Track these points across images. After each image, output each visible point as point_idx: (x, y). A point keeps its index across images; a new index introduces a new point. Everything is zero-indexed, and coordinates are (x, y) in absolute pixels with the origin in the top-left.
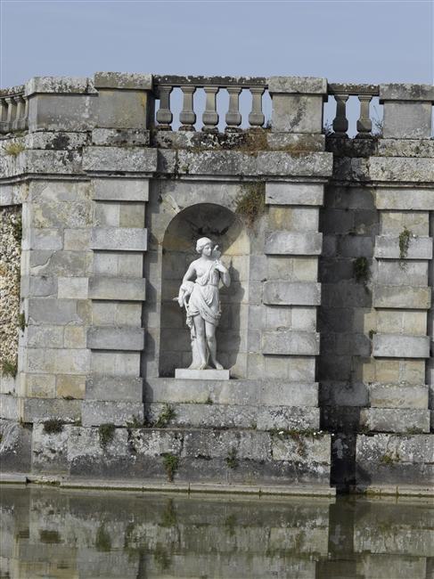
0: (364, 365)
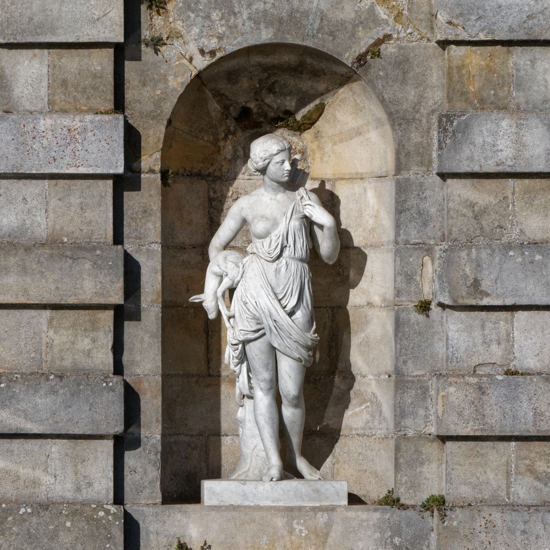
0: (351, 290)
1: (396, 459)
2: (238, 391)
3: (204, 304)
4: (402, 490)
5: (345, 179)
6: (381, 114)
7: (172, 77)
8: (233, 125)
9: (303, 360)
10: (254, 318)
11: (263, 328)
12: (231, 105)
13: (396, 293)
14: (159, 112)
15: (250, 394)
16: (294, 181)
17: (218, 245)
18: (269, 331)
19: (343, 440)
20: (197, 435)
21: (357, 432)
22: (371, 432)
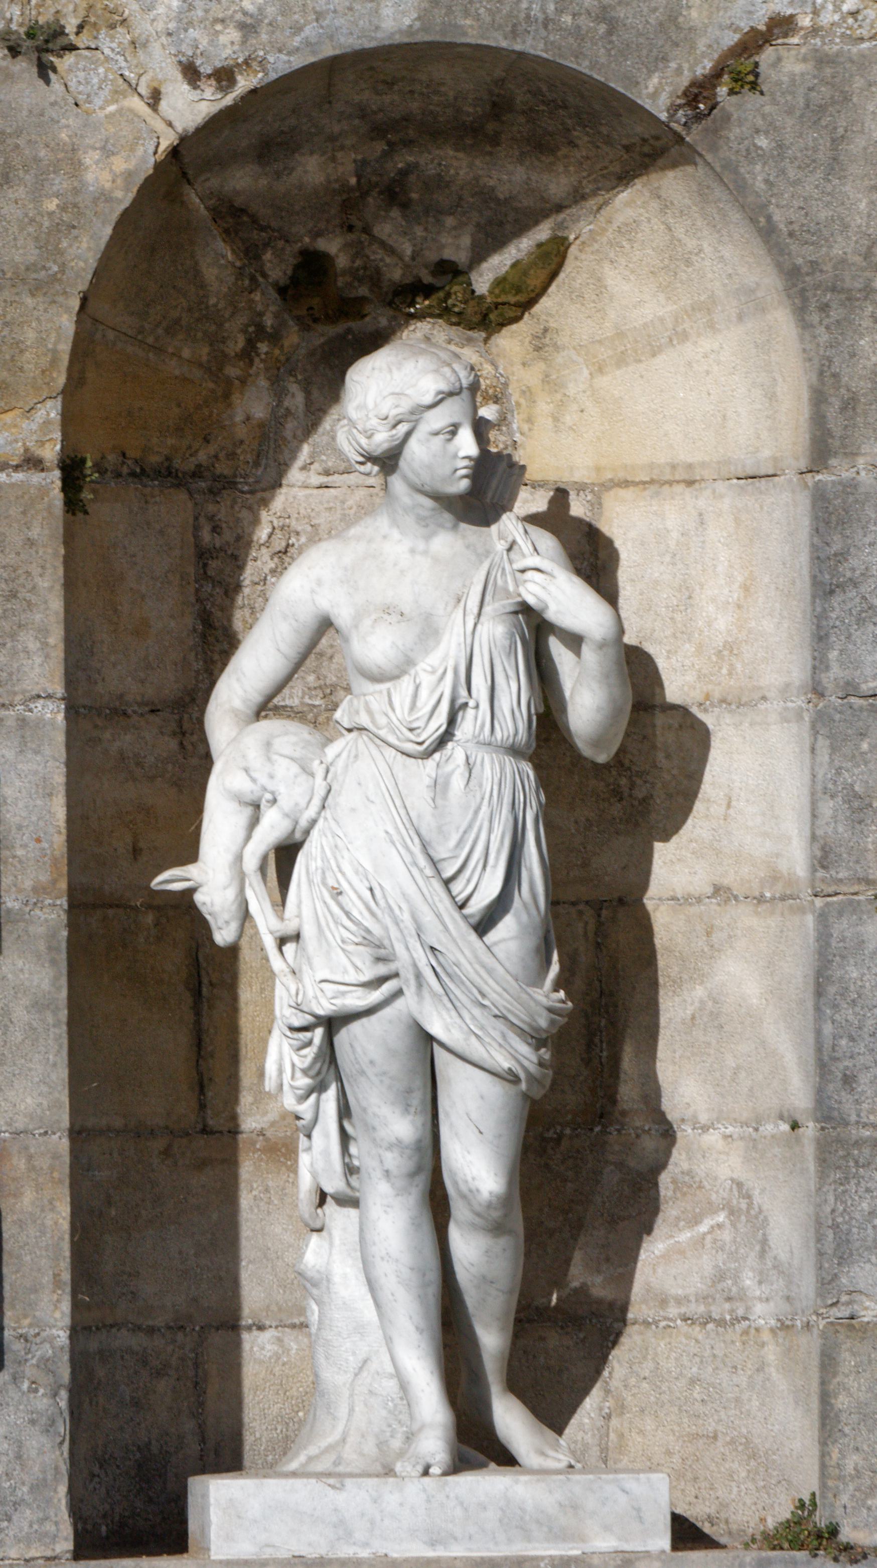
0: (658, 846)
1: (825, 1398)
2: (305, 1181)
3: (199, 898)
4: (845, 1499)
5: (635, 484)
6: (762, 277)
7: (97, 155)
8: (272, 308)
9: (522, 1075)
10: (368, 940)
11: (396, 975)
12: (266, 245)
13: (819, 854)
14: (55, 268)
15: (349, 1192)
16: (483, 494)
17: (237, 703)
18: (413, 982)
19: (637, 1339)
20: (169, 1328)
21: (683, 1310)
22: (732, 1311)
